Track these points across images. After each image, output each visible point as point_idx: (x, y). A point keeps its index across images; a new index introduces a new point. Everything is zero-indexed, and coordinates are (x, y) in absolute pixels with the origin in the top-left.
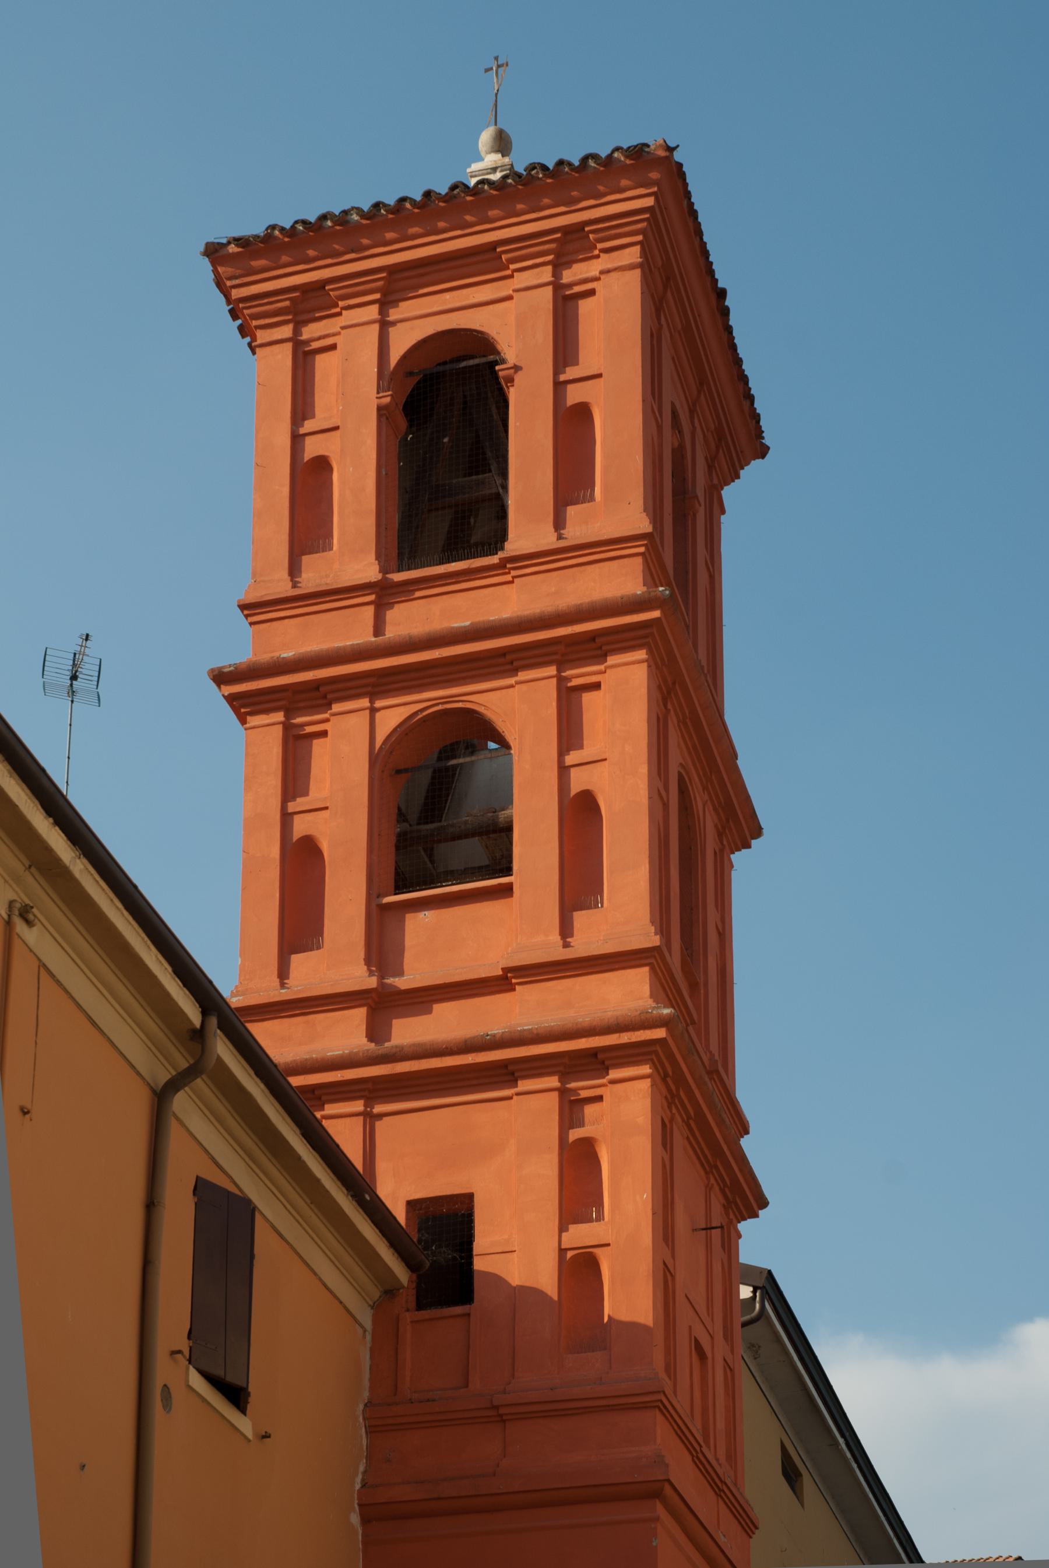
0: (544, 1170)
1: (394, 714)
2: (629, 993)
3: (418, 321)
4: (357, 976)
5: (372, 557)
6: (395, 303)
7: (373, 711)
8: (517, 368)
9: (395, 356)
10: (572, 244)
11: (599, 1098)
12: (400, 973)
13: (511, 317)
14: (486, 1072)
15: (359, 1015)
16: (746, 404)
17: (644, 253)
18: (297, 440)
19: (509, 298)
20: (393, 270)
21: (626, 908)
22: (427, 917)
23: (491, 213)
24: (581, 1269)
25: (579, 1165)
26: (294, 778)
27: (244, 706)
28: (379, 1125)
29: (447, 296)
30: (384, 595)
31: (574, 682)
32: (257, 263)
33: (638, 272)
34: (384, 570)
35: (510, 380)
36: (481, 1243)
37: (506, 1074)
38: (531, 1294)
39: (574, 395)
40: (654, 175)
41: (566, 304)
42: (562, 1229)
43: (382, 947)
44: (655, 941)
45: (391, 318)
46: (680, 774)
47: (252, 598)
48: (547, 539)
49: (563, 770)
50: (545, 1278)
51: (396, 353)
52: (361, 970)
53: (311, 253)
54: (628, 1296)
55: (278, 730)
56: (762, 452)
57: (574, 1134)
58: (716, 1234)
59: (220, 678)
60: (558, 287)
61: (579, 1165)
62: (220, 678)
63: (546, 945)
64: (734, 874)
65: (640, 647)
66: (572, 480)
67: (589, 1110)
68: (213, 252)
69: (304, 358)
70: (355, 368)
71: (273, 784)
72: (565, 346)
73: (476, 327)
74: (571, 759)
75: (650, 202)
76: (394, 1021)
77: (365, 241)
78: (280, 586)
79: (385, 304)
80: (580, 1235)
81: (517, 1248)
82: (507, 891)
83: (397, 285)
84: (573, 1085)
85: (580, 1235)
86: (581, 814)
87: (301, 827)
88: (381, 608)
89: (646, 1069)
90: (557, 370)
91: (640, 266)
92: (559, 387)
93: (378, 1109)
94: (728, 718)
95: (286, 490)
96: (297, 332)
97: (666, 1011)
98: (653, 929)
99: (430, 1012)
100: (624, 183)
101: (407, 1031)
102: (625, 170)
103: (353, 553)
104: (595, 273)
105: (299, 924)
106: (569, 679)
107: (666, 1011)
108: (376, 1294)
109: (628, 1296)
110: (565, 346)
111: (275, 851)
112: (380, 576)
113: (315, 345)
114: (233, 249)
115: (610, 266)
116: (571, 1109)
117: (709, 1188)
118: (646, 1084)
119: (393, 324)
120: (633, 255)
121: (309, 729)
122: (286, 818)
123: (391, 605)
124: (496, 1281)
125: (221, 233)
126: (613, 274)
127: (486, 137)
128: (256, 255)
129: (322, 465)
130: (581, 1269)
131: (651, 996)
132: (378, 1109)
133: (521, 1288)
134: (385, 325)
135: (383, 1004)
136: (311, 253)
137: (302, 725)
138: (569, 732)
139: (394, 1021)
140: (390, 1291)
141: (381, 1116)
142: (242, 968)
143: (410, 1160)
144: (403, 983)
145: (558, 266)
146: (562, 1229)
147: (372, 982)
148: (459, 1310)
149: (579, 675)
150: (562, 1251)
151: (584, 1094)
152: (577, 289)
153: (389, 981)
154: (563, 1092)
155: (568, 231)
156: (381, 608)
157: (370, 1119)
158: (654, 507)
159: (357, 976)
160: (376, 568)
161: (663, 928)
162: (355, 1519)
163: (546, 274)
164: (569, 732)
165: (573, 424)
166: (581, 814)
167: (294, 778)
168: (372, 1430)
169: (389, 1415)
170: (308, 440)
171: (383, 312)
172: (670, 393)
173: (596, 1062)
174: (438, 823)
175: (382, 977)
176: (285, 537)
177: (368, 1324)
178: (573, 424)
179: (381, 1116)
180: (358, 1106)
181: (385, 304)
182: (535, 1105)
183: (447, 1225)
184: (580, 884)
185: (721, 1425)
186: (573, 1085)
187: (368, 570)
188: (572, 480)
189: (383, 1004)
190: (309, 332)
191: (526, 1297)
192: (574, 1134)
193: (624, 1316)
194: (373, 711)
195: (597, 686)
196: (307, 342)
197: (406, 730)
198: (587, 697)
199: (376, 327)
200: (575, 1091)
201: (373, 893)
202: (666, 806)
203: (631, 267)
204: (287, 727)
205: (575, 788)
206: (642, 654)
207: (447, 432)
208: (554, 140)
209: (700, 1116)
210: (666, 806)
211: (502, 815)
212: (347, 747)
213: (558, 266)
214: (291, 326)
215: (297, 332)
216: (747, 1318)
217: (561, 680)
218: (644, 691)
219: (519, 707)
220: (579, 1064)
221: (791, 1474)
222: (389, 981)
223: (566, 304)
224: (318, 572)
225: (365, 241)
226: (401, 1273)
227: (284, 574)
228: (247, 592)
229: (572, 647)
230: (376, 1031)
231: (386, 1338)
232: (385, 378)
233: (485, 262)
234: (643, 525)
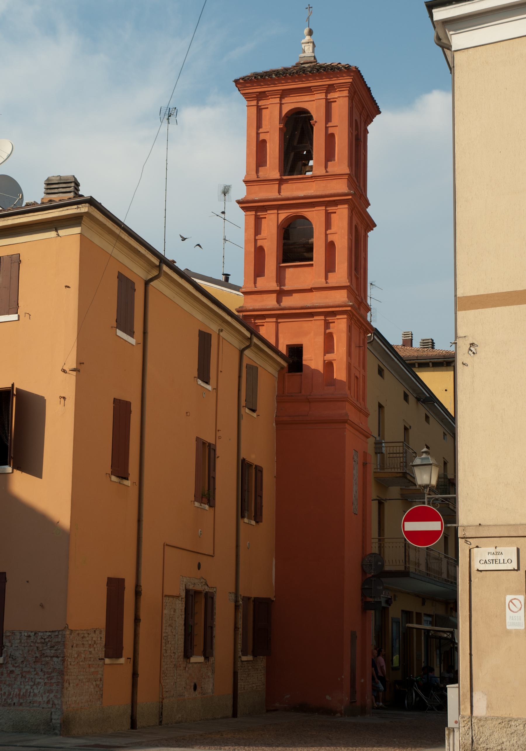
0: (320, 340)
1: (284, 215)
2: (341, 297)
3: (291, 103)
4: (274, 286)
5: (278, 171)
6: (284, 98)
7: (278, 214)
8: (316, 122)
9: (284, 113)
10: (330, 88)
11: (334, 322)
12: (284, 285)
13: (314, 104)
14: (306, 314)
15: (275, 295)
16: (375, 106)
17: (349, 93)
18: (258, 134)
19: (314, 100)
20: (283, 90)
21: (341, 275)
22: (291, 270)
23: (310, 79)
24: (329, 365)
25: (329, 338)
26: (257, 230)
27: (244, 209)
28: (279, 324)
29: (298, 97)
30: (281, 182)
31: (329, 211)
32: (247, 85)
33: (347, 98)
34: (281, 176)
35: (314, 125)
36: (305, 357)
37: (312, 315)
38: (316, 371)
39: (331, 131)
40: (352, 74)
41: (328, 104)
42: (325, 355)
43: (280, 279)
44: (348, 284)
45: (283, 102)
46: (356, 225)
47: (246, 180)
48: (323, 172)
49: (326, 235)
50: (320, 368)
51: (284, 113)
52: (275, 284)
53: (262, 84)
54: (340, 373)
55: (253, 217)
56: (379, 112)
57: (328, 331)
58: (361, 348)
59: (239, 202)
60: (326, 99)
61: (329, 338)
62: (239, 202)
63: (321, 282)
64: (369, 239)
65: (346, 204)
66: (330, 156)
67: (331, 325)
68: (236, 82)
69: (259, 110)
70: (273, 114)
71: (252, 231)
72: (328, 117)
73: (305, 107)
74: (328, 232)
75: (351, 80)
76: (283, 298)
77: (276, 82)
78: (254, 177)
79: (281, 98)
80: (329, 357)
81: (313, 359)
82: (312, 265)
83: (284, 94)
84: (328, 318)
85: (329, 357)
86: (330, 247)
87: (259, 243)
88: (280, 185)
89: (345, 316)
90: (326, 124)
91: (348, 96)
92: (327, 128)
93: (279, 321)
94: (368, 196)
95: (255, 149)
96: (258, 103)
97: (351, 304)
98: (348, 281)
99: (292, 295)
100: (344, 75)
101: (288, 302)
102: (345, 72)
103: (272, 169)
104: (336, 96)
105: (259, 271)
106: (328, 210)
107: (351, 304)
108: (279, 369)
109: (340, 373)
110: (328, 117)
111: (253, 250)
112: (280, 177)
113: (262, 107)
114: (241, 81)
115: (340, 96)
116: (327, 325)
117: (360, 333)
118: (345, 320)
119: (283, 104)
120: (346, 93)
121: (261, 216)
122: (256, 241)
123: (282, 184)
124: (308, 367)
125: (237, 77)
126: (341, 98)
127: (306, 31)
128: (248, 83)
129: (264, 141)
130: (329, 365)
131: (348, 297)
132: (279, 321)
133: (314, 369)
134: (281, 104)
135: (281, 294)
136: (262, 84)
137: (260, 215)
138: (328, 225)
139: (283, 298)
140: (282, 368)
141: (280, 322)
142: (244, 280)
143: (286, 335)
144: (286, 288)
145: (327, 93)
146: (325, 355)
147: (278, 288)
148: (299, 373)
149: (331, 209)
150: (324, 361)
151: (330, 321)
152: (331, 100)
153: (282, 287)
154: (325, 320)
155: (329, 85)
156: (280, 185)
157: (277, 323)
158: (350, 165)
159: (274, 286)
160: (279, 174)
161: (351, 281)
162: (274, 424)
163: (323, 96)
164: (328, 225)
165: (330, 138)
166: (330, 247)
167: (257, 230)
168: (278, 402)
169: (282, 398)
170: (261, 135)
171: (281, 100)
172: (356, 116)
173: (334, 314)
174: (295, 247)
175: (280, 286)
176: (255, 162)
177: (277, 376)
178: (330, 138)
179: (280, 322)
180: (274, 320)
181: (281, 98)
182: (318, 323)
183: (296, 351)
184: (330, 267)
185: (361, 393)
186: (328, 318)
187: (276, 174)
188: (330, 156)
189: (281, 294)
190: (261, 103)
191: (315, 372)
192: (328, 331)
193: (339, 378)
194: (278, 214)
195: (335, 213)
196: (260, 106)
197: (286, 219)
198: (332, 215)
199: (279, 104)
200: (328, 320)
201: (278, 263)
202: (351, 240)
203: (346, 97)
204: (256, 216)
205: (329, 240)
206: (346, 206)
207: (297, 131)
208: (325, 59)
209: (358, 320)
210: (351, 240)
211: (310, 241)
212: (271, 223)
213: (327, 93)
214: (256, 101)
215: (258, 103)
216: (369, 341)
217: (326, 210)
218: (347, 216)
219: (315, 216)
220: (329, 314)
221: (381, 372)
222: (282, 287)
223: (328, 104)
224: (264, 173)
225: (276, 82)
226: (285, 364)
227: (254, 173)
228: (245, 177)
229: (328, 202)
230: (279, 301)
231: (281, 380)
232: (281, 120)
233: (308, 90)
234: (347, 171)
